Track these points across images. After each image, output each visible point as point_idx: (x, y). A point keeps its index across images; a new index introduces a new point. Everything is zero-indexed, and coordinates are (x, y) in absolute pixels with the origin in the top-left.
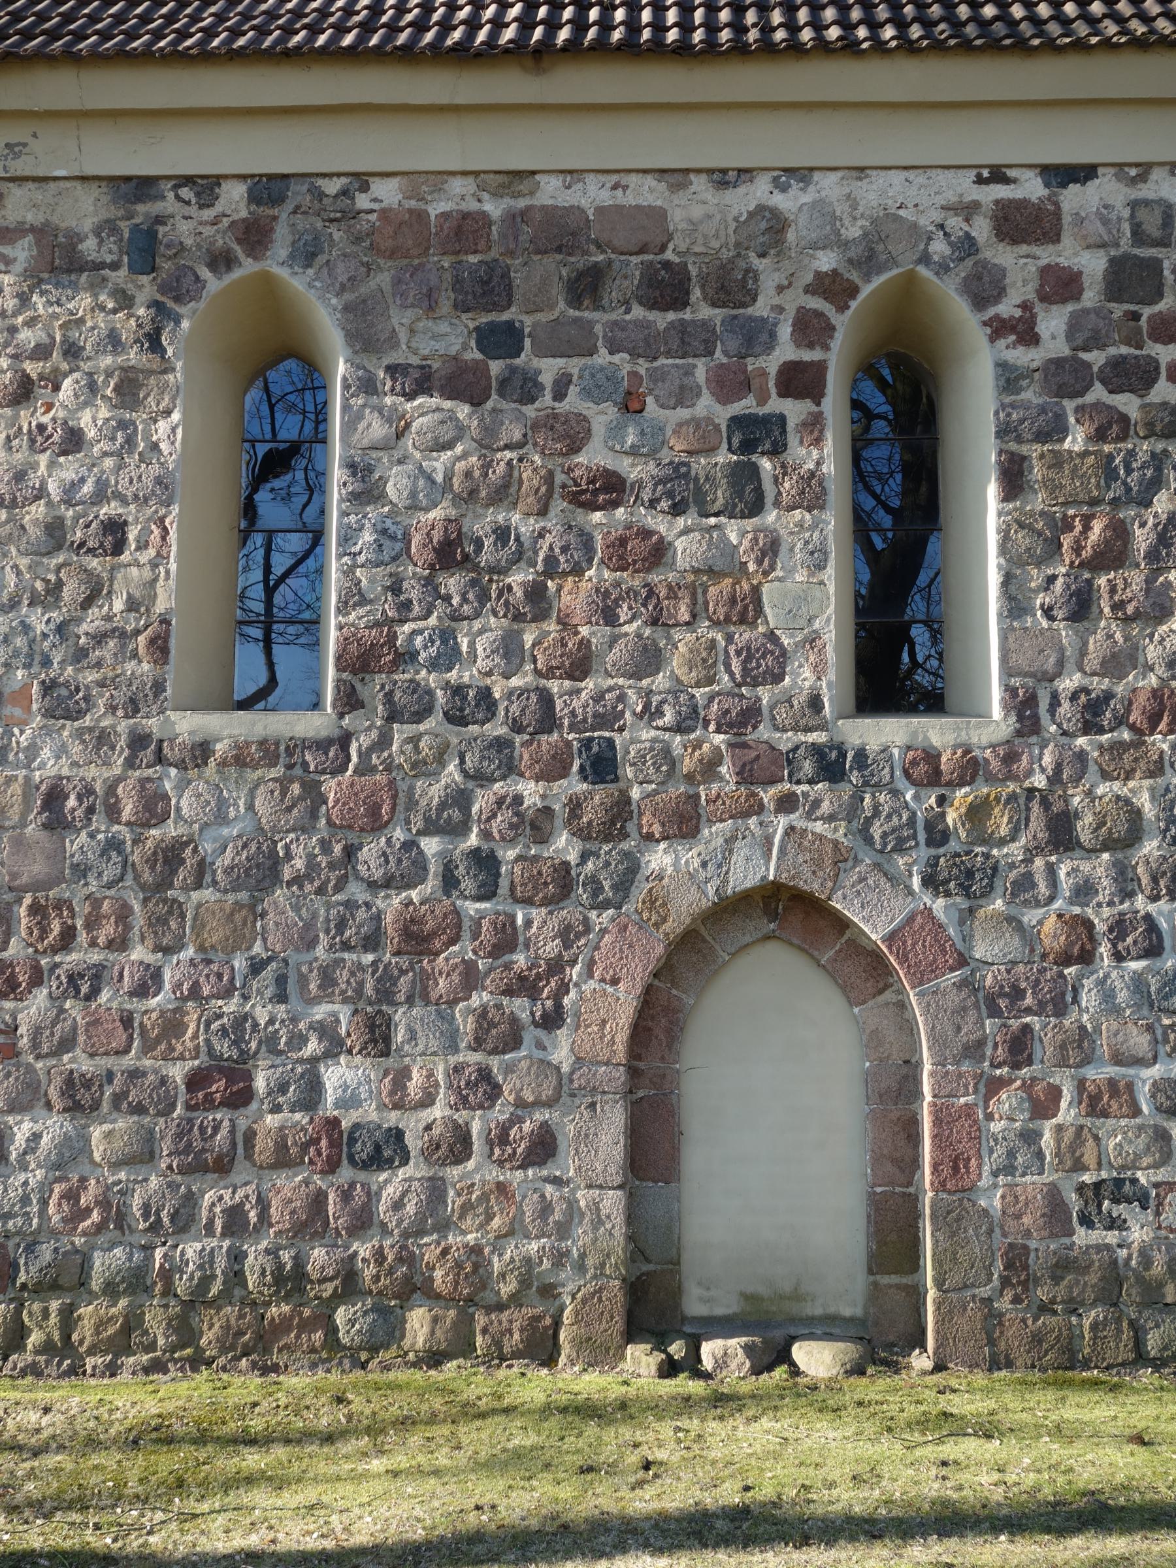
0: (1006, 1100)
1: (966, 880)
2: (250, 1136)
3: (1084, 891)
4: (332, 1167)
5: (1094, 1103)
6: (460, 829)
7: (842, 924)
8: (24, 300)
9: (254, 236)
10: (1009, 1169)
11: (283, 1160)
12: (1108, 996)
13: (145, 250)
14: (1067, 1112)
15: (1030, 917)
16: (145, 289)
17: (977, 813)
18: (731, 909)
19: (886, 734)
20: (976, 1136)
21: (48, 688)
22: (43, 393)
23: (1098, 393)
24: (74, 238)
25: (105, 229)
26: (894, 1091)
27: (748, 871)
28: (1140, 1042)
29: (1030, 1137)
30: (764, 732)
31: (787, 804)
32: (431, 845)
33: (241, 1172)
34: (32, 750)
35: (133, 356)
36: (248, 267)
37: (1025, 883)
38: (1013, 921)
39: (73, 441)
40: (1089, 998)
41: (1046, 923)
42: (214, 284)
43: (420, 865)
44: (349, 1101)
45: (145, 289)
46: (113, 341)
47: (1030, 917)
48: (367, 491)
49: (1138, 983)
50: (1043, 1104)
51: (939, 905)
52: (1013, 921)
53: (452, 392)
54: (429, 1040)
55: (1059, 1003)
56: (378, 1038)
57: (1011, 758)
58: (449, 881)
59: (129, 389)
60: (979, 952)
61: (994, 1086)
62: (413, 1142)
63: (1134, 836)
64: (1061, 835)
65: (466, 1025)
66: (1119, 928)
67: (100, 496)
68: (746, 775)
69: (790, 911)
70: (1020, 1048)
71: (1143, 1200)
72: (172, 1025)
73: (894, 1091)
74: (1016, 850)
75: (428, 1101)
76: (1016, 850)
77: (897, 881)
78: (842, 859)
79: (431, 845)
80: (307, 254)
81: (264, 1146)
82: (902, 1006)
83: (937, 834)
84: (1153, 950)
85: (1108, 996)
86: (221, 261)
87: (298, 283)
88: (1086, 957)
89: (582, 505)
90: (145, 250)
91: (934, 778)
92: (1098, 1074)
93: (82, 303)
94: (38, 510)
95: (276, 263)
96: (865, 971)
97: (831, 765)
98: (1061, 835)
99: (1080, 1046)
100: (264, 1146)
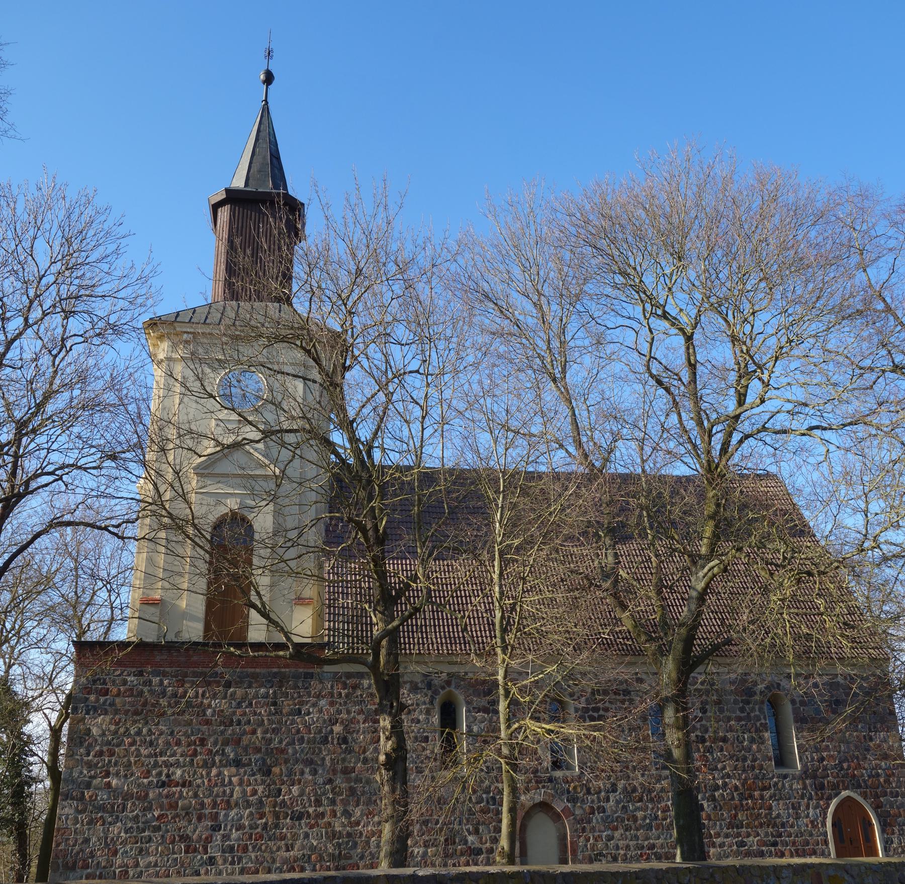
0: (582, 839)
1: (573, 800)
2: (456, 850)
3: (593, 801)
4: (470, 856)
5: (596, 840)
6: (488, 793)
7: (553, 808)
8: (409, 695)
9: (448, 683)
10: (583, 851)
11: (462, 854)
12: (597, 820)
13: (429, 685)
14: (591, 841)
15: (584, 806)
16: (430, 693)
17: (575, 788)
18: (535, 806)
19: (558, 774)
20: (577, 845)
21: (416, 768)
22: (413, 713)
23: (591, 713)
24: (417, 683)
25: (422, 681)
26: (563, 838)
27: (538, 798)
28: (603, 828)
29: (586, 846)
30: (539, 774)
31: (544, 787)
32: (484, 796)
33: (455, 857)
34: (414, 779)
35: (428, 706)
36: (448, 689)
37: (583, 800)
38: (581, 807)
39: (418, 721)
40: (594, 821)
41: (586, 807)
42: (442, 692)
43: (482, 799)
44: (473, 843)
45: (430, 693)
46: (424, 703)
47: (584, 806)
48: (60, 819)
49: (602, 818)
50: (588, 840)
51: (569, 805)
52: (581, 807)
53: (484, 712)
54: (486, 831)
55: (589, 821)
56: (477, 832)
57: (580, 778)
58: (488, 802)
59: (428, 712)
60: (577, 813)
61: (580, 837)
62: (484, 850)
63: (600, 792)
64: (589, 792)
65: (492, 829)
66: (599, 808)
67: (424, 732)
68: (537, 782)
69: (544, 806)
70: (584, 830)
71: (604, 856)
72: (441, 829)
73: (563, 838)
74: (581, 795)
75: (486, 843)
76: (581, 795)
77: (562, 800)
78: (553, 796)
79: (484, 796)
80: (458, 687)
81: (458, 853)
82: (563, 823)
83: (569, 792)
84: (604, 812)
85: (597, 820)
86: (443, 688)
87: (457, 692)
88: (593, 813)
89: (451, 751)
90: (429, 685)
91: (568, 782)
92: (596, 834)
93: (419, 696)
94: (413, 734)
95: (452, 688)
96: (557, 818)
97: (550, 780)
98: (589, 792)
99: (593, 829)
100: (458, 853)
